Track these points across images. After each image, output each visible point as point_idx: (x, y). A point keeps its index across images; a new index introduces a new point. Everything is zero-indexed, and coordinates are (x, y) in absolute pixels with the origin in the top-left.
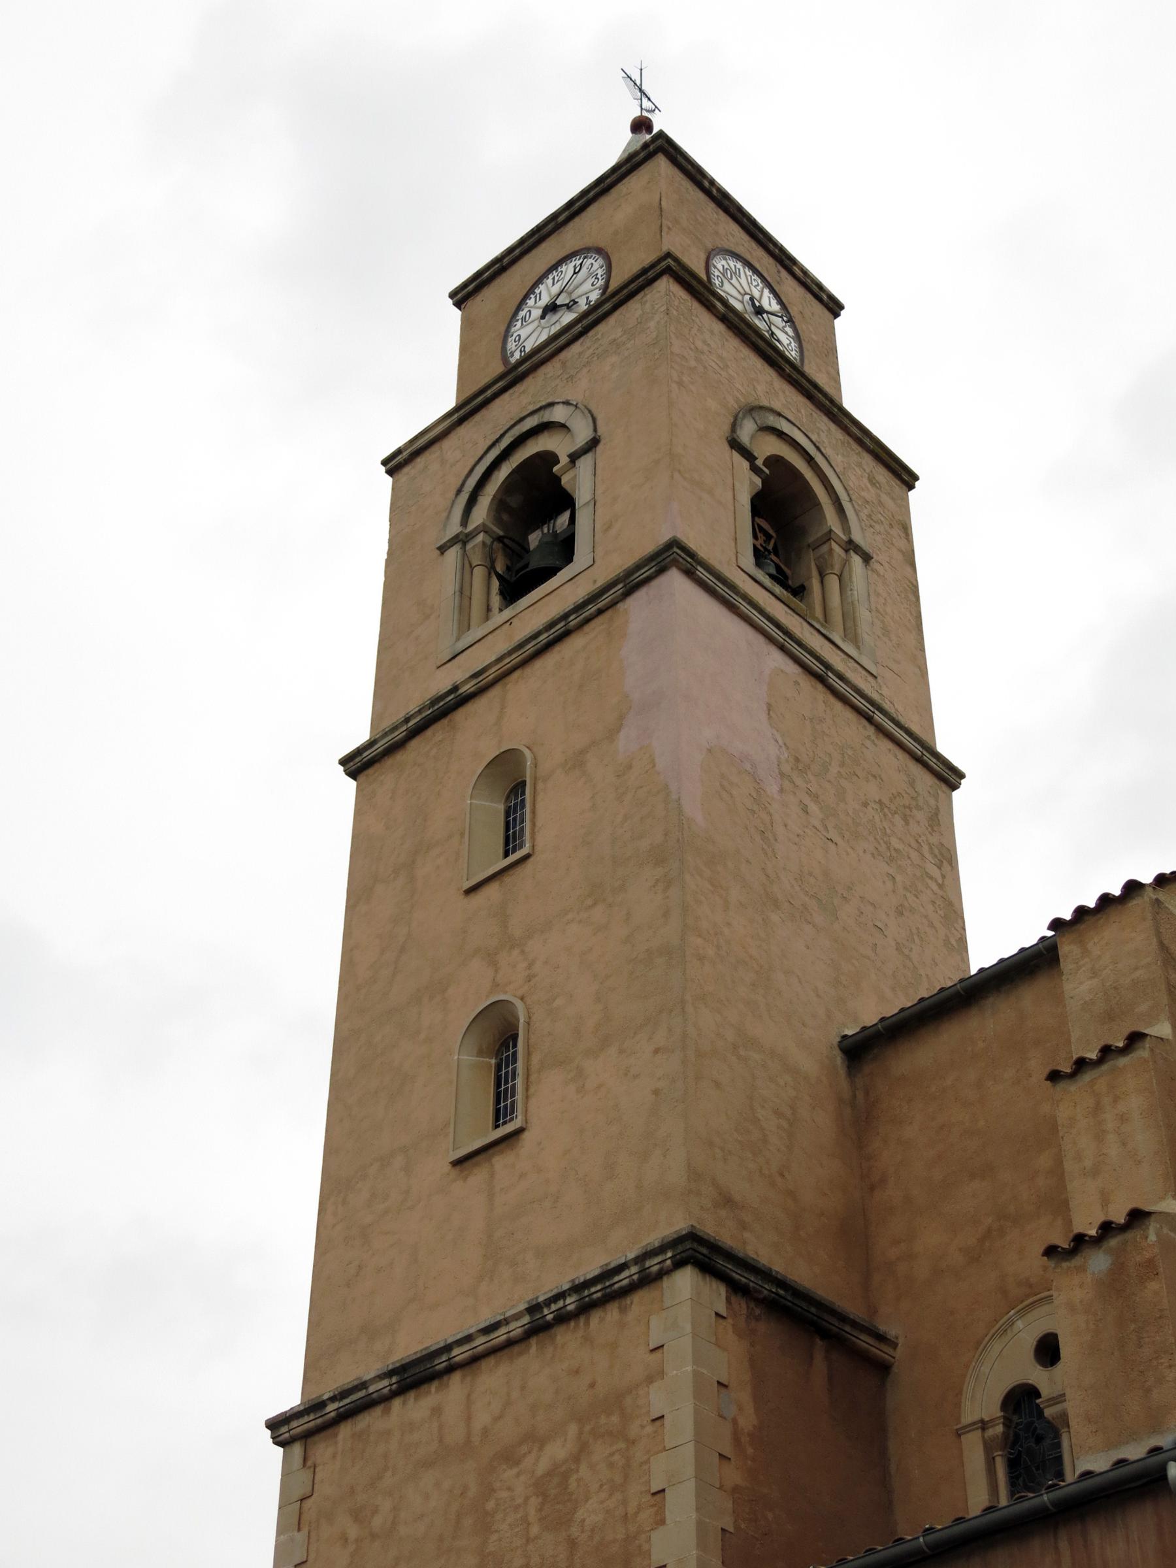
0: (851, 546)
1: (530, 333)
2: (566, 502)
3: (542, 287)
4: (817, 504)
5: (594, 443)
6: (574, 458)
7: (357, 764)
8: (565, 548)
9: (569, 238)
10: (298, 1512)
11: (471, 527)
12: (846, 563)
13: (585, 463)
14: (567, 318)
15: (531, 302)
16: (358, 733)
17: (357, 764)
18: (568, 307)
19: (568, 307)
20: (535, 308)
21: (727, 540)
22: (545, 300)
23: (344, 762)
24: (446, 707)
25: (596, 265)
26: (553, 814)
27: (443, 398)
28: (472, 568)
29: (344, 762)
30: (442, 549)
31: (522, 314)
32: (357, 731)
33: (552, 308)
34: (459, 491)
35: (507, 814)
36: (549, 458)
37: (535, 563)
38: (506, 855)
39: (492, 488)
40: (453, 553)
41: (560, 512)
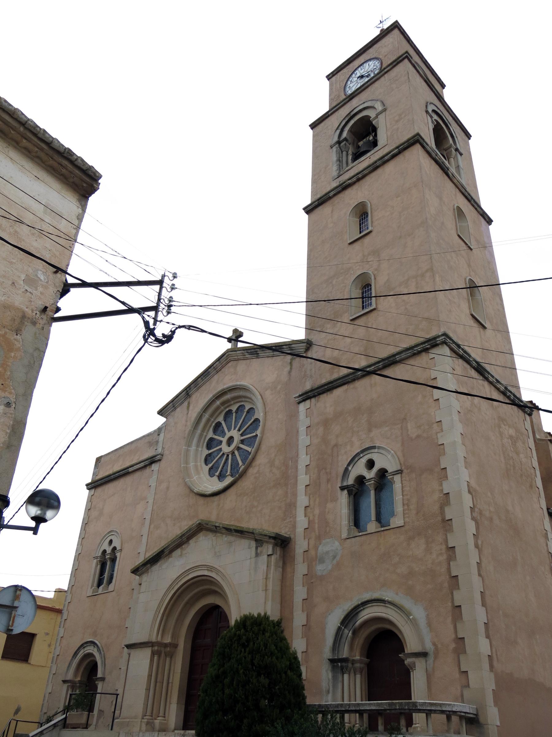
0: (457, 150)
1: (354, 85)
2: (375, 129)
3: (357, 71)
4: (447, 137)
5: (385, 110)
6: (377, 117)
7: (308, 210)
8: (375, 144)
9: (371, 52)
10: (90, 500)
11: (341, 139)
12: (456, 155)
13: (381, 117)
14: (367, 79)
15: (354, 75)
16: (308, 201)
17: (308, 210)
18: (367, 76)
19: (367, 76)
20: (354, 78)
21: (430, 139)
22: (358, 75)
23: (304, 209)
24: (344, 187)
25: (377, 63)
26: (376, 220)
27: (325, 108)
28: (342, 152)
29: (304, 209)
30: (332, 147)
31: (350, 80)
32: (307, 201)
33: (362, 77)
34: (337, 129)
35: (360, 221)
36: (368, 117)
37: (362, 150)
38: (360, 233)
39: (352, 122)
40: (334, 149)
41: (368, 134)
